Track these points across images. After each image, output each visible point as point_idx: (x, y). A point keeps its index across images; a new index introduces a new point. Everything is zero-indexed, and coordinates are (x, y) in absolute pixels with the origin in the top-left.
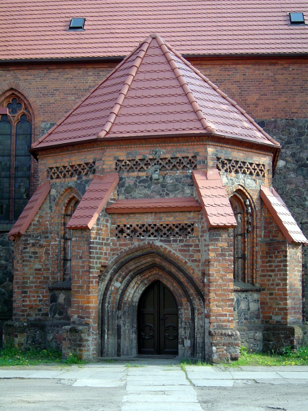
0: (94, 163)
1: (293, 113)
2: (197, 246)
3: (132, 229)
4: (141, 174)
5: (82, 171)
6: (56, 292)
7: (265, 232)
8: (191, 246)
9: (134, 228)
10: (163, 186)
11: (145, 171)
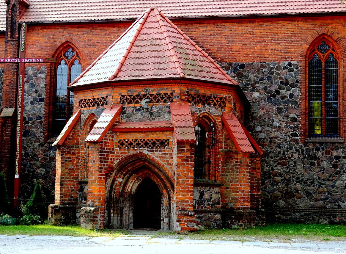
1: (265, 58)
3: (129, 142)
4: (136, 105)
5: (100, 103)
6: (82, 185)
7: (225, 145)
8: (167, 154)
9: (131, 142)
10: (152, 113)
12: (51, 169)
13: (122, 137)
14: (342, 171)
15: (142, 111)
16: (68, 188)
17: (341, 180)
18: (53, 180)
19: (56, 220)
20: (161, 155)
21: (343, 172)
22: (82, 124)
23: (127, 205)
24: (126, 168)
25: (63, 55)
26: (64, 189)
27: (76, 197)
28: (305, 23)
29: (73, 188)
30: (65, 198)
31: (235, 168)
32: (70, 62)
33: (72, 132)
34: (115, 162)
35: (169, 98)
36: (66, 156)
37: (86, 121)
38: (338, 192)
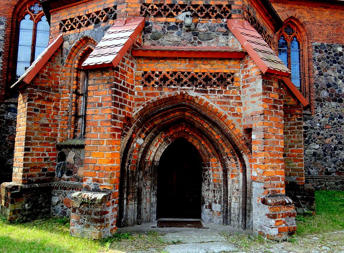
0: (115, 7)
2: (238, 98)
3: (161, 76)
4: (169, 20)
6: (64, 150)
8: (232, 98)
11: (173, 16)
12: (8, 134)
13: (149, 67)
14: (310, 140)
15: (179, 29)
16: (39, 155)
17: (310, 149)
18: (9, 146)
19: (14, 212)
20: (221, 98)
21: (311, 141)
22: (66, 57)
23: (148, 184)
24: (152, 122)
25: (28, 9)
26: (30, 158)
27: (51, 169)
28: (276, 5)
29: (47, 156)
30: (33, 173)
31: (298, 128)
32: (36, 17)
33: (47, 67)
34: (134, 109)
35: (225, 12)
36: (36, 104)
37: (73, 51)
38: (307, 160)
